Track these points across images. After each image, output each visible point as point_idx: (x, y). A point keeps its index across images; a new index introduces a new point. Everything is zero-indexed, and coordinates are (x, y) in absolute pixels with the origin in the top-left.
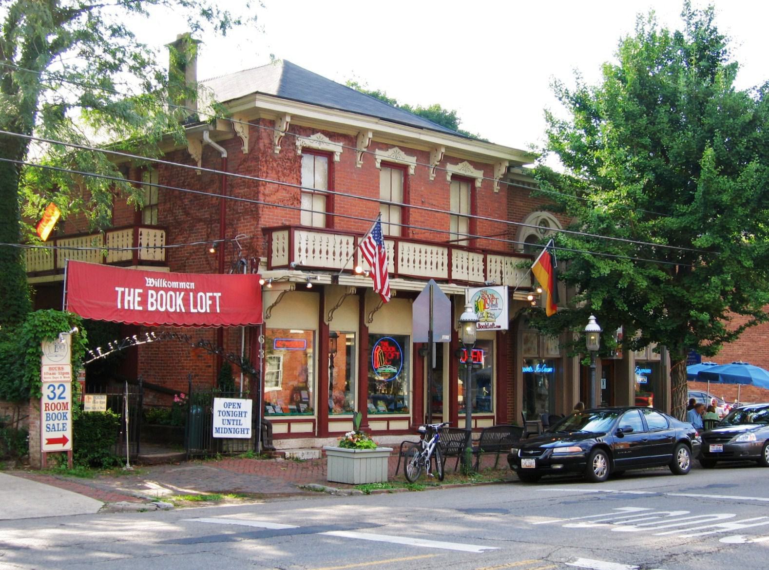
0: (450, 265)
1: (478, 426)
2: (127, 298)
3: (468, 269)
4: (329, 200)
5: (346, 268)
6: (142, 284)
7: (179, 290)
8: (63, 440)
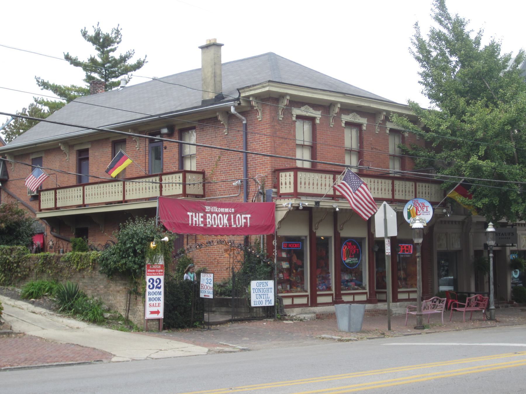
0: (393, 191)
1: (410, 298)
2: (194, 219)
3: (309, 185)
4: (313, 149)
5: (328, 194)
6: (203, 210)
7: (226, 213)
8: (158, 312)
